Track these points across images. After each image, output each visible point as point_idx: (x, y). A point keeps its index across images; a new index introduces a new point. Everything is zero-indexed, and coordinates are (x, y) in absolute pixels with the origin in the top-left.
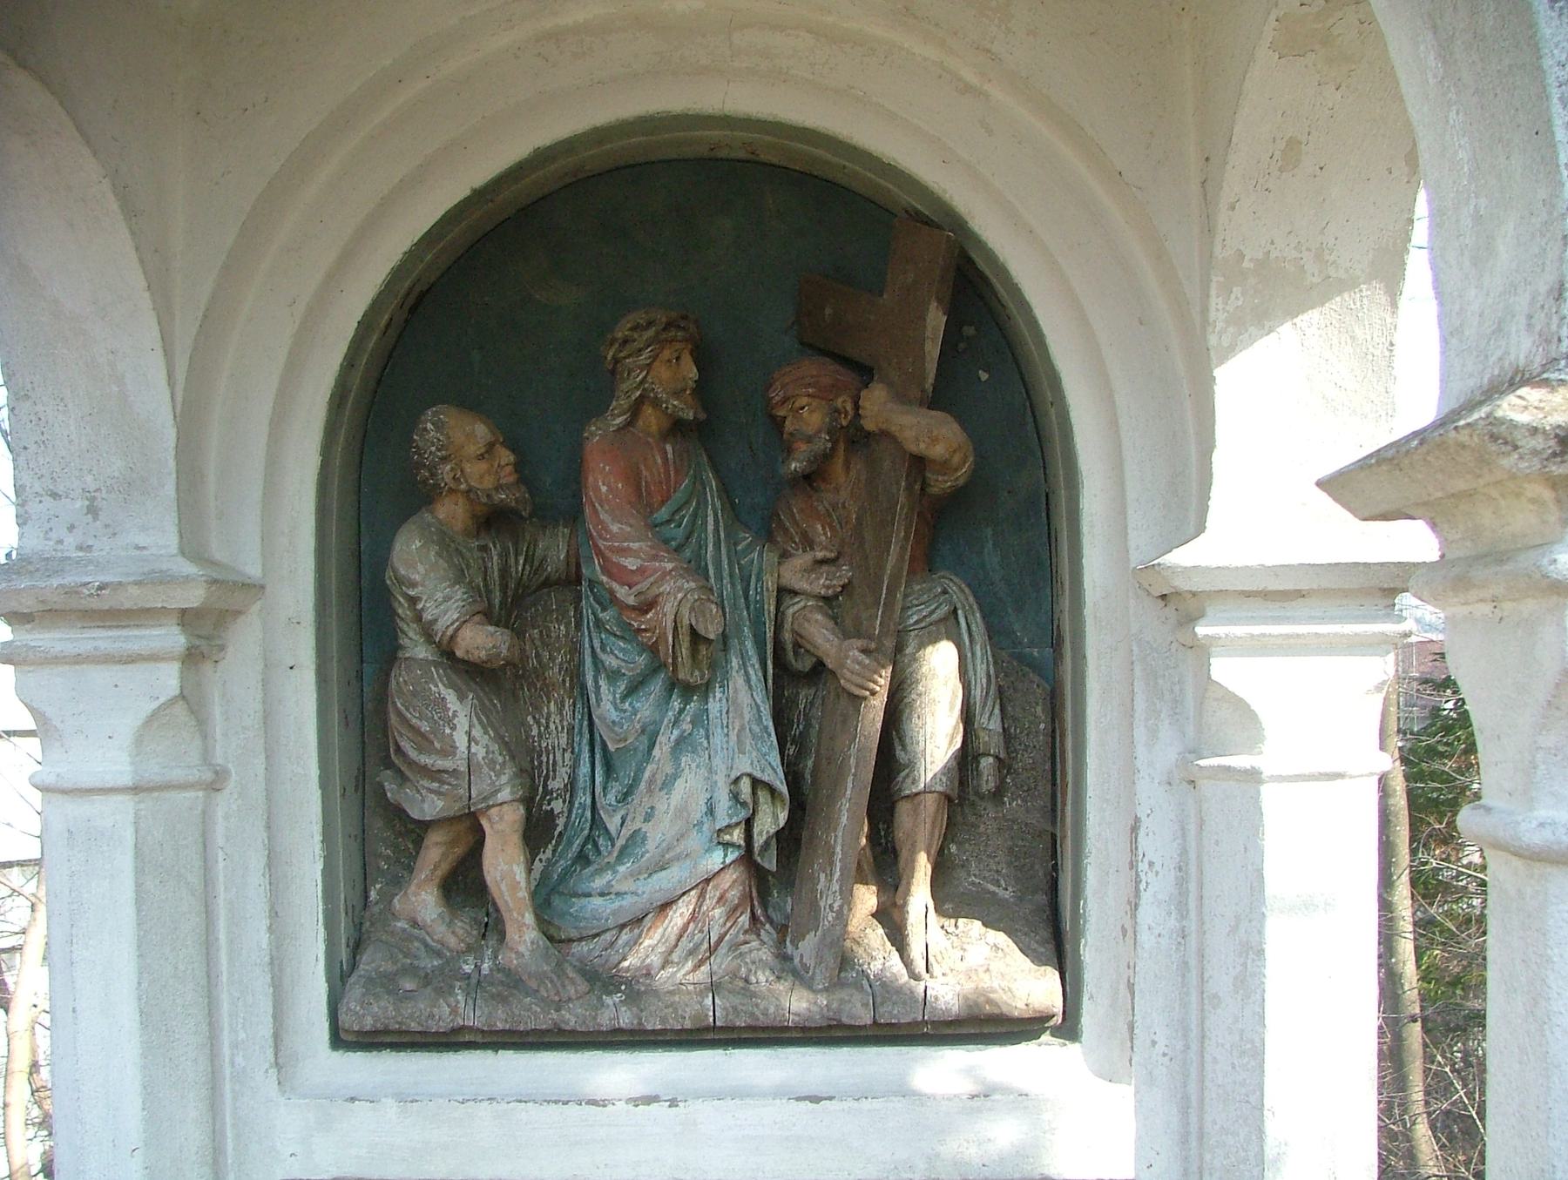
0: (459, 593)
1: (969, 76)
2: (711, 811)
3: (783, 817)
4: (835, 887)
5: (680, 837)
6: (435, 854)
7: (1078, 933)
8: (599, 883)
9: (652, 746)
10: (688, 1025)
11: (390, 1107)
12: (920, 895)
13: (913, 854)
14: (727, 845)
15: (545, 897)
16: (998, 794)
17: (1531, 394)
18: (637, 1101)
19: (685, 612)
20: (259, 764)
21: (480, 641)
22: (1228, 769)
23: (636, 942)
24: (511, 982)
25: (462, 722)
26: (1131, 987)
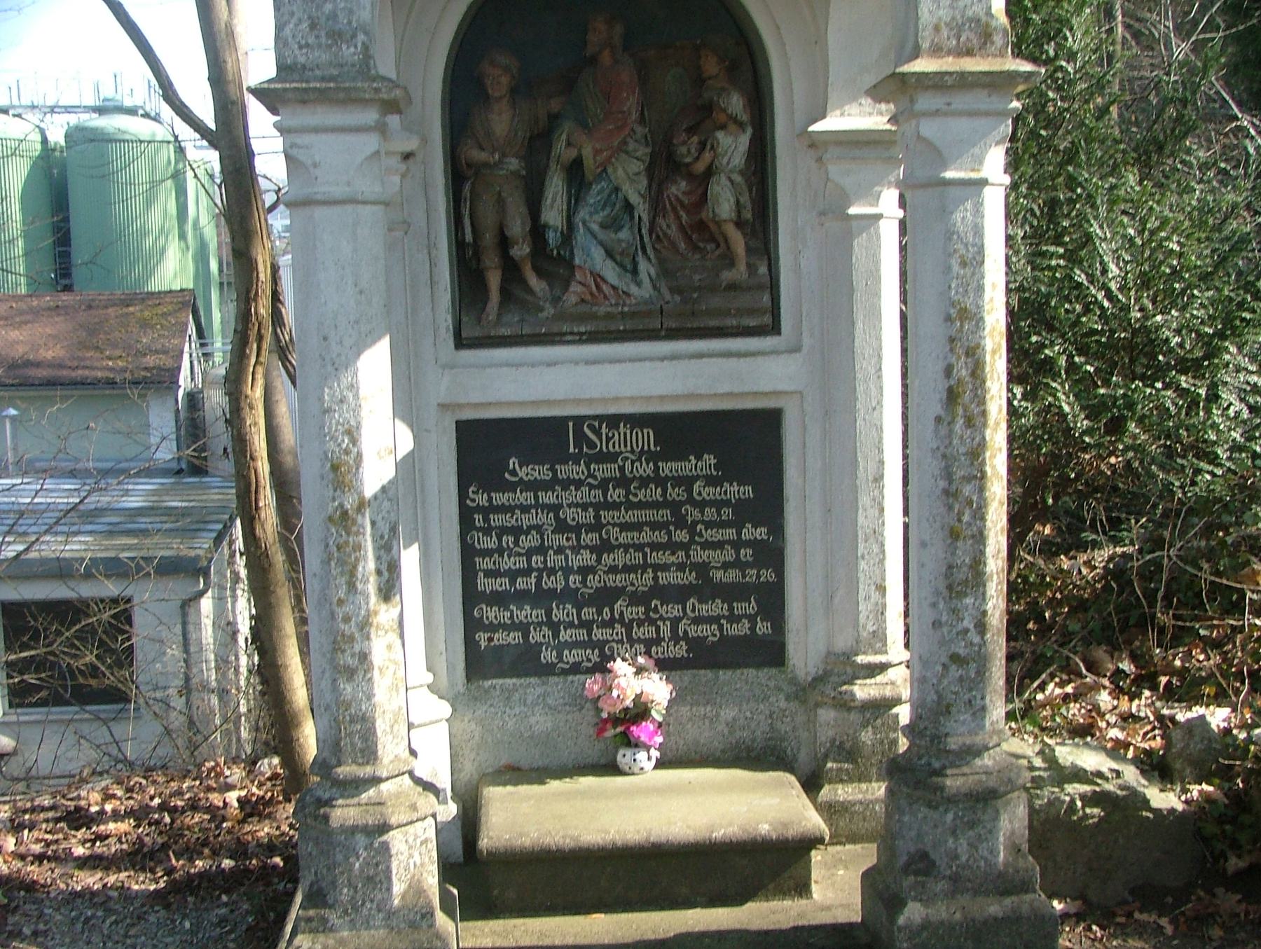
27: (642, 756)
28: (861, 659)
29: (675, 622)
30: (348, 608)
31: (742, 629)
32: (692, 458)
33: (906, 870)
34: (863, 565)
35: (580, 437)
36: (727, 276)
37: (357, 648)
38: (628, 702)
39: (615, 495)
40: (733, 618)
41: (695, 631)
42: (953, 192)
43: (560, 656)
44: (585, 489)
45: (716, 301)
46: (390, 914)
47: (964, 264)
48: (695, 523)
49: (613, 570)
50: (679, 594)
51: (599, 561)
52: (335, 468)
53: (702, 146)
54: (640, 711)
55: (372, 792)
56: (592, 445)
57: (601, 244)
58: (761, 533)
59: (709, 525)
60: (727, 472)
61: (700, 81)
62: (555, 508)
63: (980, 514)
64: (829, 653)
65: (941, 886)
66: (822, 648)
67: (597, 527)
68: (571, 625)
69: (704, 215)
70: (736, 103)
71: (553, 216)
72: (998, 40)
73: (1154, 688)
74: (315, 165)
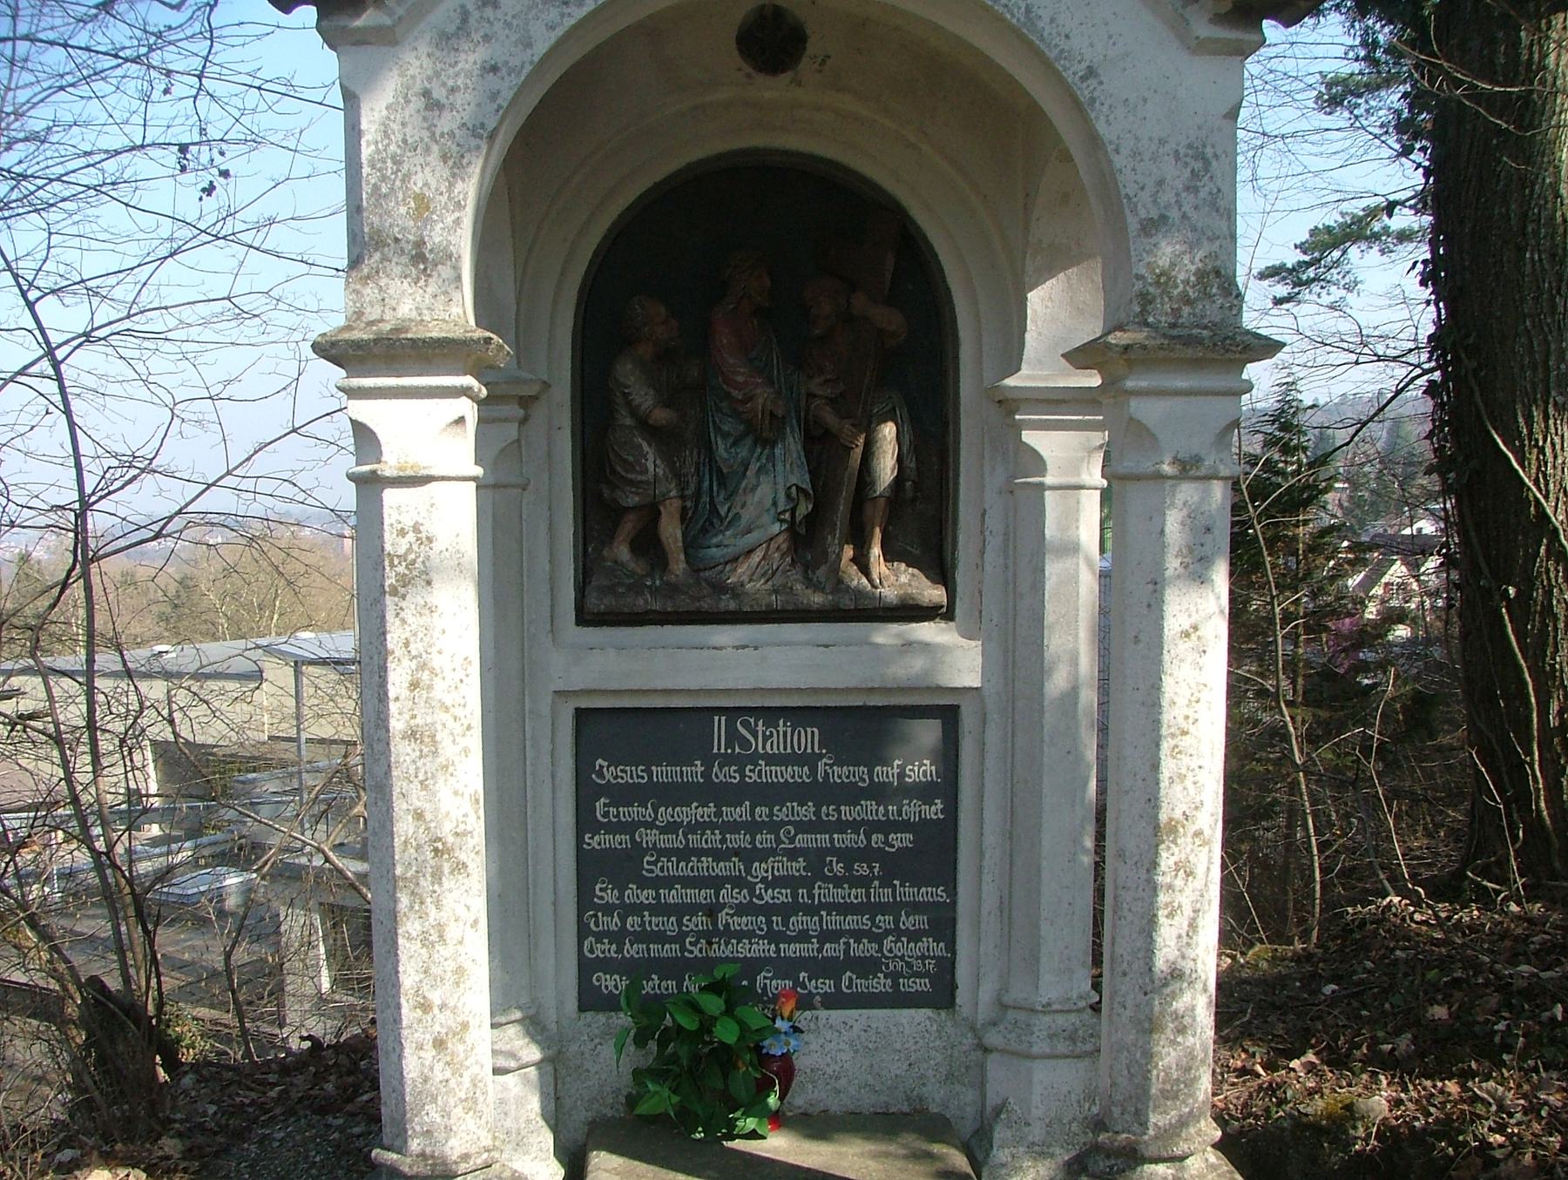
0: (652, 392)
1: (913, 140)
2: (775, 504)
3: (810, 507)
4: (836, 541)
5: (758, 517)
6: (628, 526)
7: (954, 567)
8: (715, 541)
9: (746, 470)
10: (764, 608)
11: (612, 653)
12: (876, 551)
13: (873, 528)
14: (782, 521)
15: (691, 545)
16: (914, 499)
17: (1118, 334)
18: (737, 648)
19: (769, 403)
20: (546, 475)
21: (661, 416)
22: (1029, 483)
23: (735, 570)
24: (673, 590)
25: (651, 457)
26: (980, 592)
32: (846, 886)
56: (745, 744)
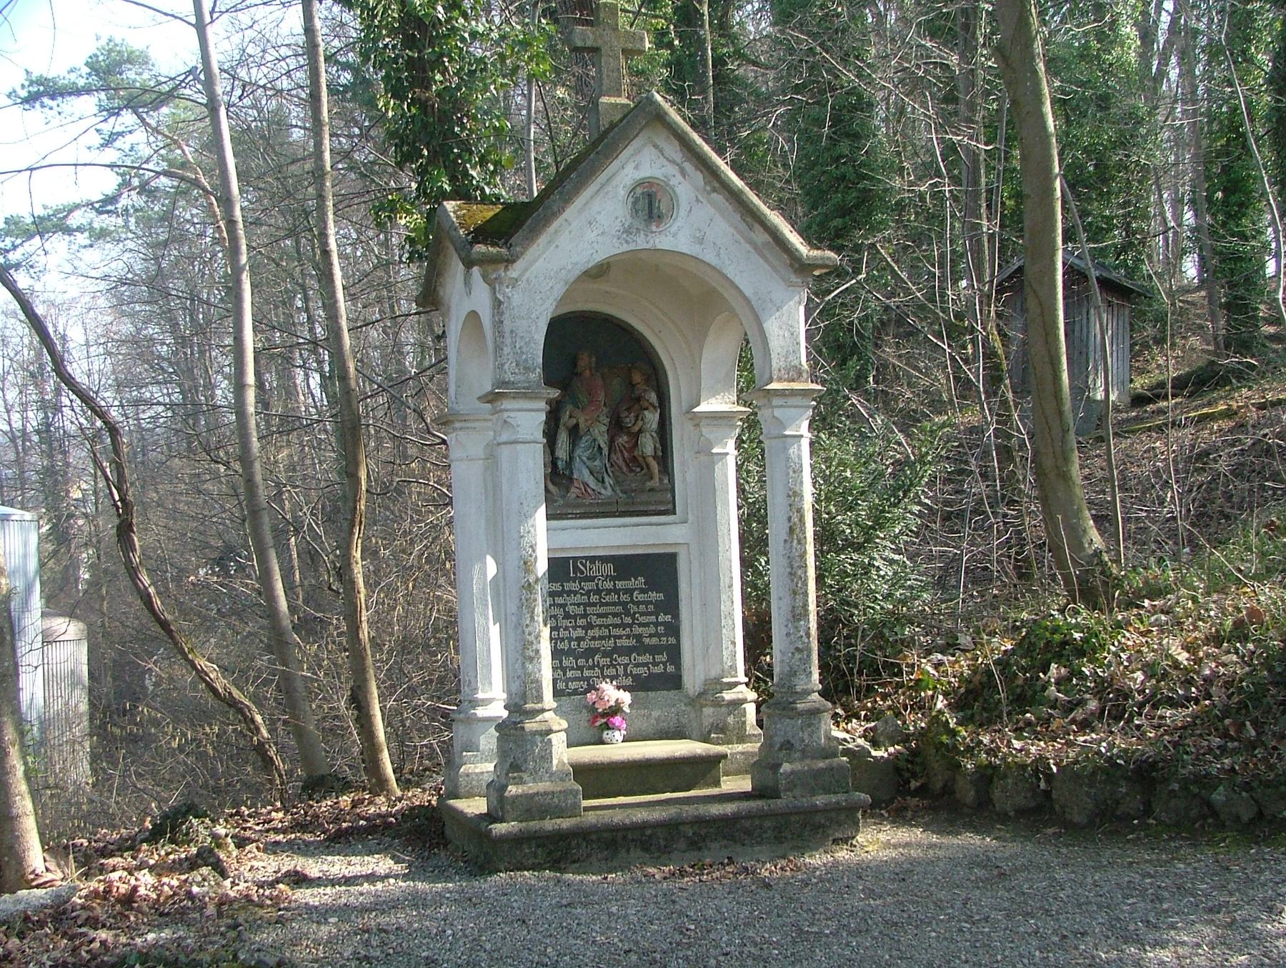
27: (617, 733)
28: (725, 680)
29: (626, 666)
30: (530, 629)
31: (658, 670)
33: (780, 749)
34: (724, 631)
35: (576, 568)
36: (649, 484)
37: (534, 647)
38: (612, 703)
39: (594, 598)
40: (655, 664)
41: (636, 671)
42: (789, 440)
43: (567, 686)
44: (579, 596)
45: (644, 497)
46: (552, 774)
47: (794, 472)
48: (635, 613)
49: (593, 638)
50: (628, 651)
51: (586, 633)
52: (525, 563)
53: (637, 418)
54: (616, 710)
55: (540, 717)
57: (588, 467)
58: (668, 618)
59: (642, 614)
60: (651, 586)
61: (632, 386)
62: (563, 606)
63: (805, 584)
64: (706, 681)
65: (798, 755)
66: (703, 678)
67: (585, 616)
68: (572, 668)
69: (636, 453)
70: (653, 397)
71: (562, 453)
72: (805, 375)
73: (858, 718)
74: (518, 426)
